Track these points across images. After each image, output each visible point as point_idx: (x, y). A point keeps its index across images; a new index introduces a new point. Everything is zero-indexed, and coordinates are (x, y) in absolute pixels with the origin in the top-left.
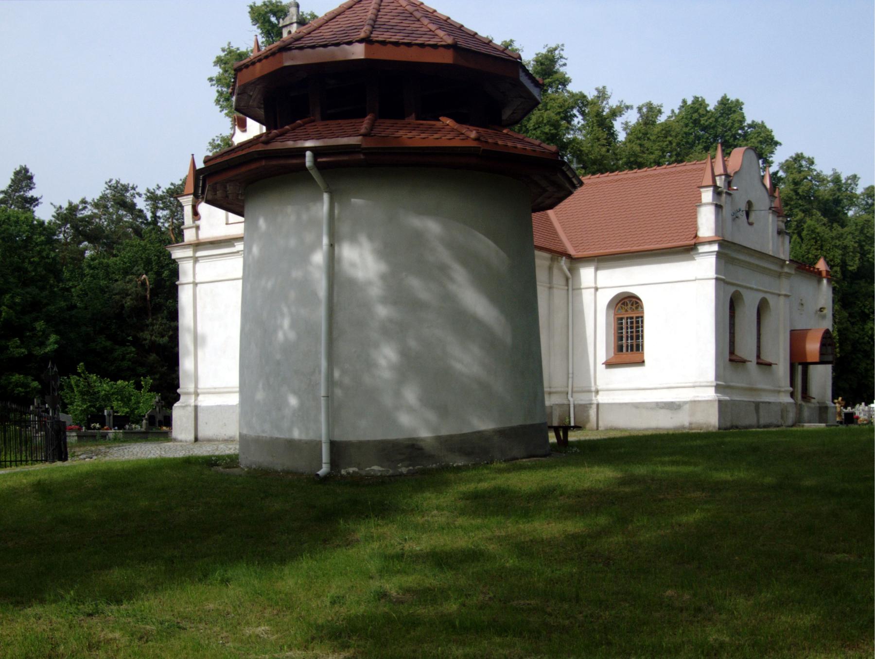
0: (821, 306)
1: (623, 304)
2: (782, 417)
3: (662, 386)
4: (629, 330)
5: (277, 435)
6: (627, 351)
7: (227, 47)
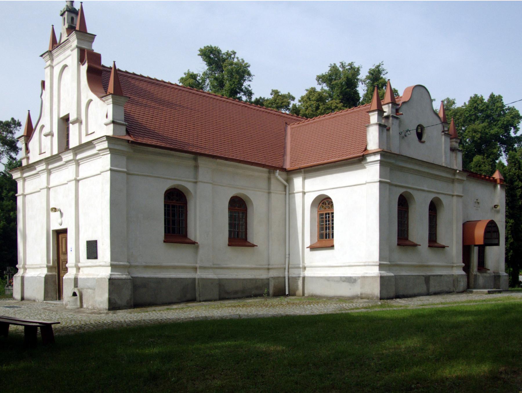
0: (496, 204)
1: (323, 203)
2: (454, 286)
3: (345, 265)
7: (187, 72)
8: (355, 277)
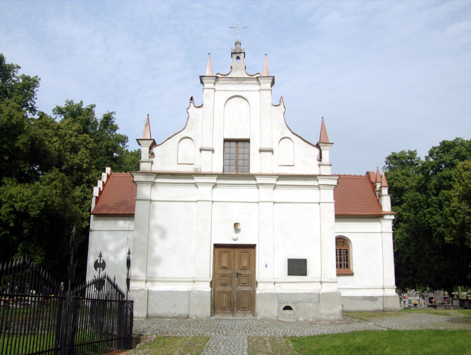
4: (345, 256)
6: (345, 267)
8: (376, 296)
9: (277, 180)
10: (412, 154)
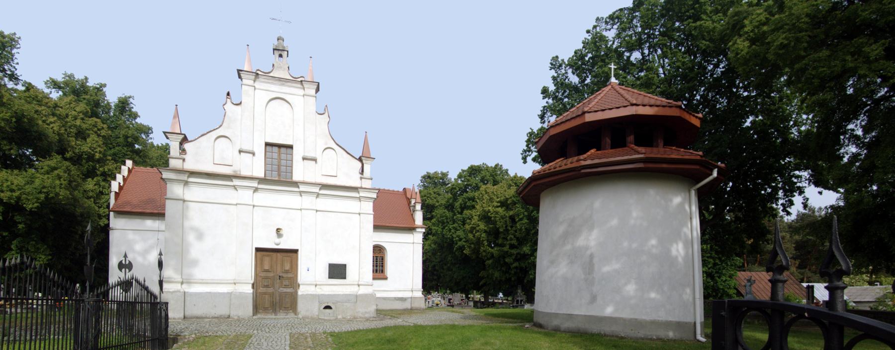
5: (670, 319)
9: (320, 189)
10: (445, 175)
